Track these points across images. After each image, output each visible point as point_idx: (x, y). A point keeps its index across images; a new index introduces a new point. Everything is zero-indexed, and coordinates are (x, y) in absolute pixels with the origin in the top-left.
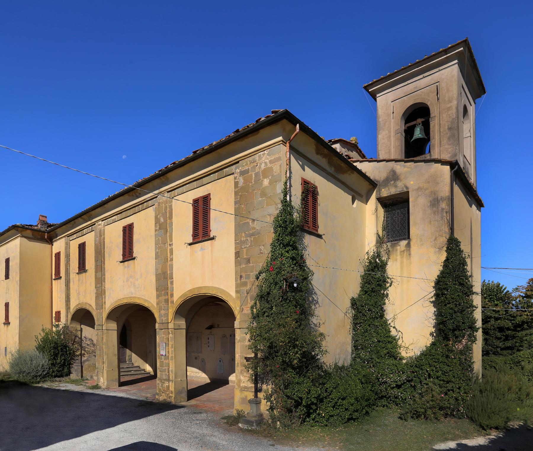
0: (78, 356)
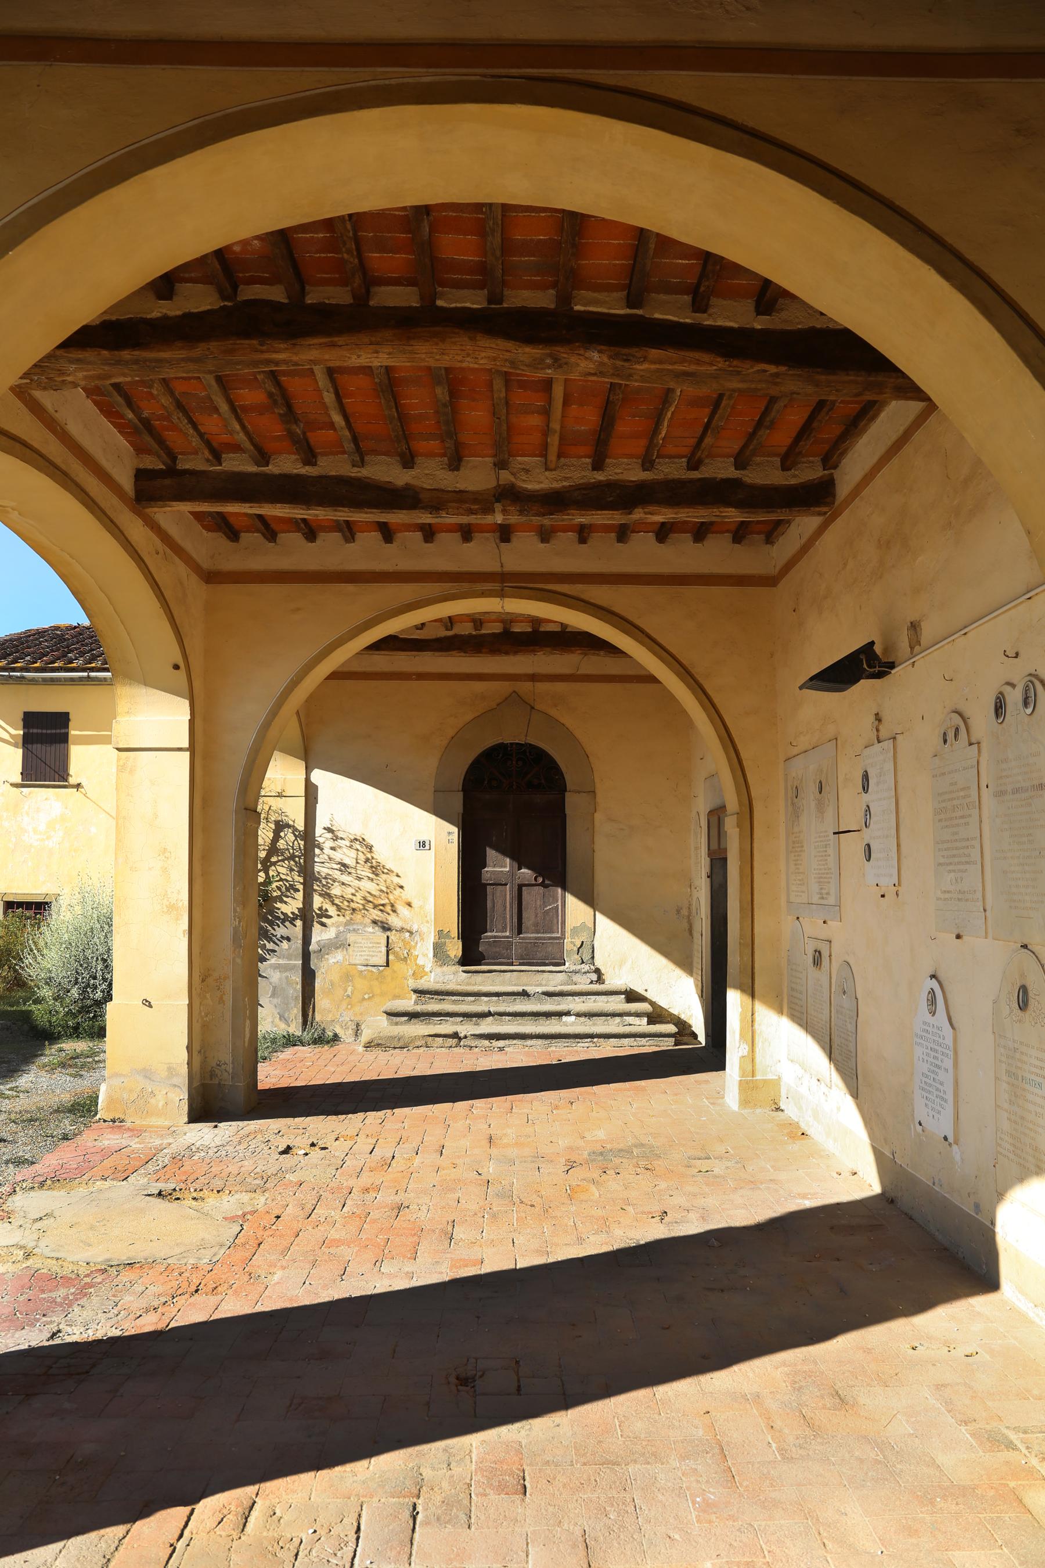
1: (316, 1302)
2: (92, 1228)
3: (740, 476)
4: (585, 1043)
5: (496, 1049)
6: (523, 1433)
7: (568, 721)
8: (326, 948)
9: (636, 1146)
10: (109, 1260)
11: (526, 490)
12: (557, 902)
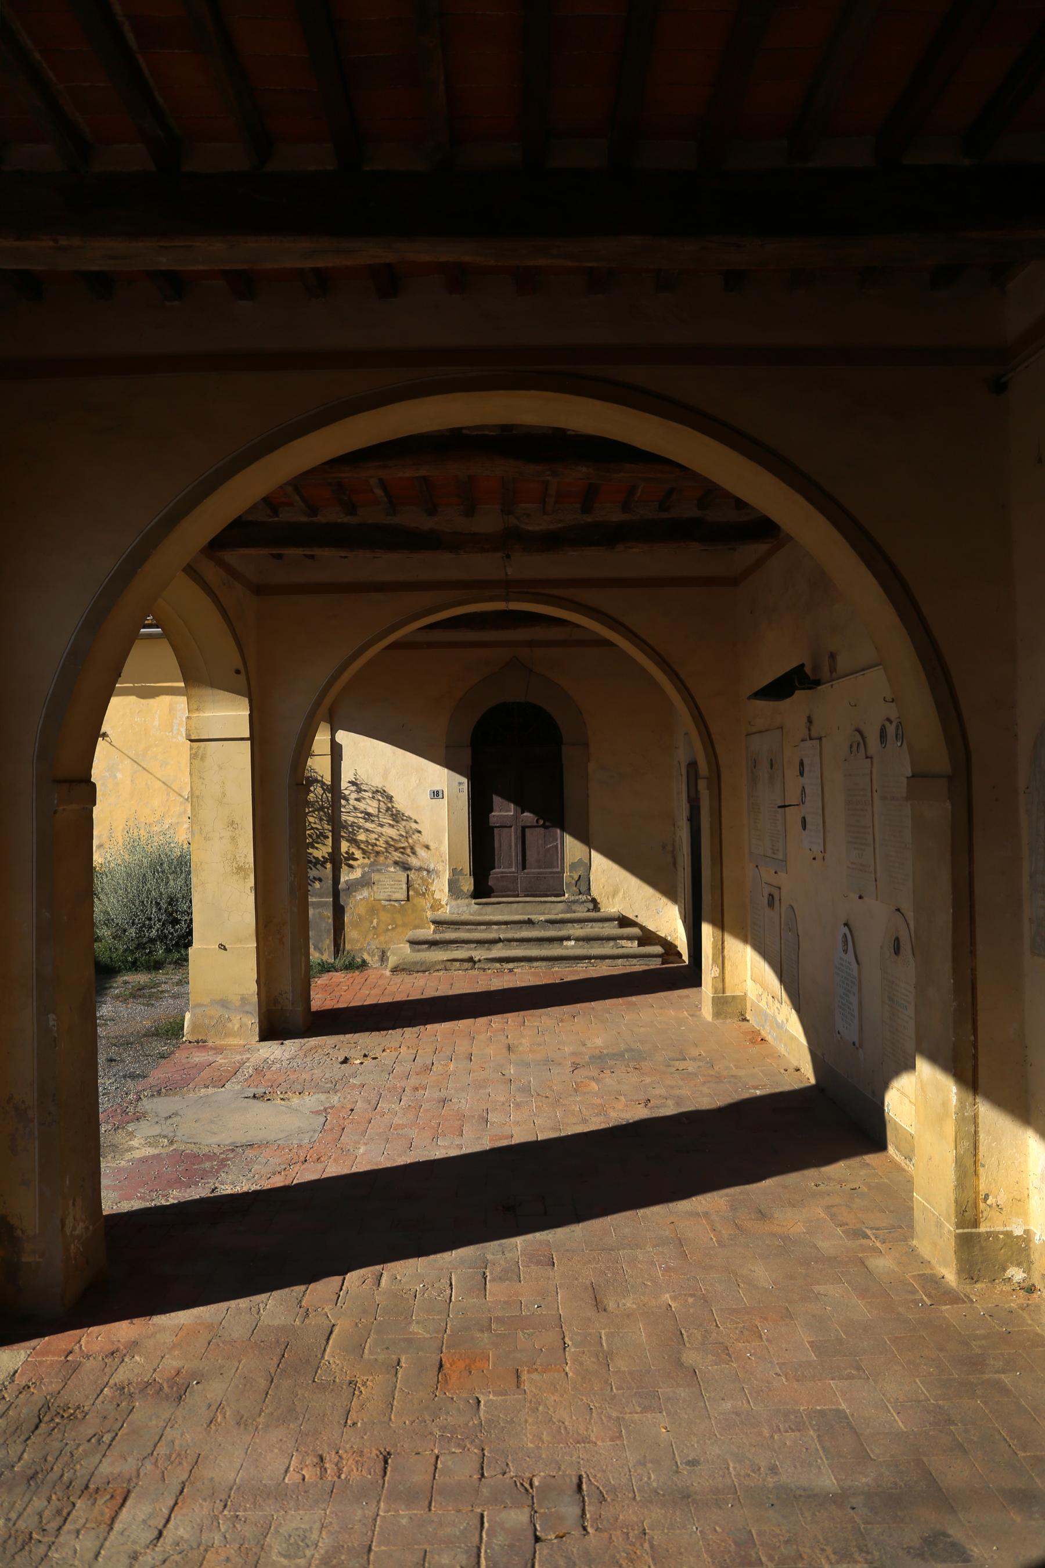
0: (323, 864)
1: (395, 1165)
2: (212, 1122)
6: (550, 1235)
8: (354, 886)
12: (557, 840)
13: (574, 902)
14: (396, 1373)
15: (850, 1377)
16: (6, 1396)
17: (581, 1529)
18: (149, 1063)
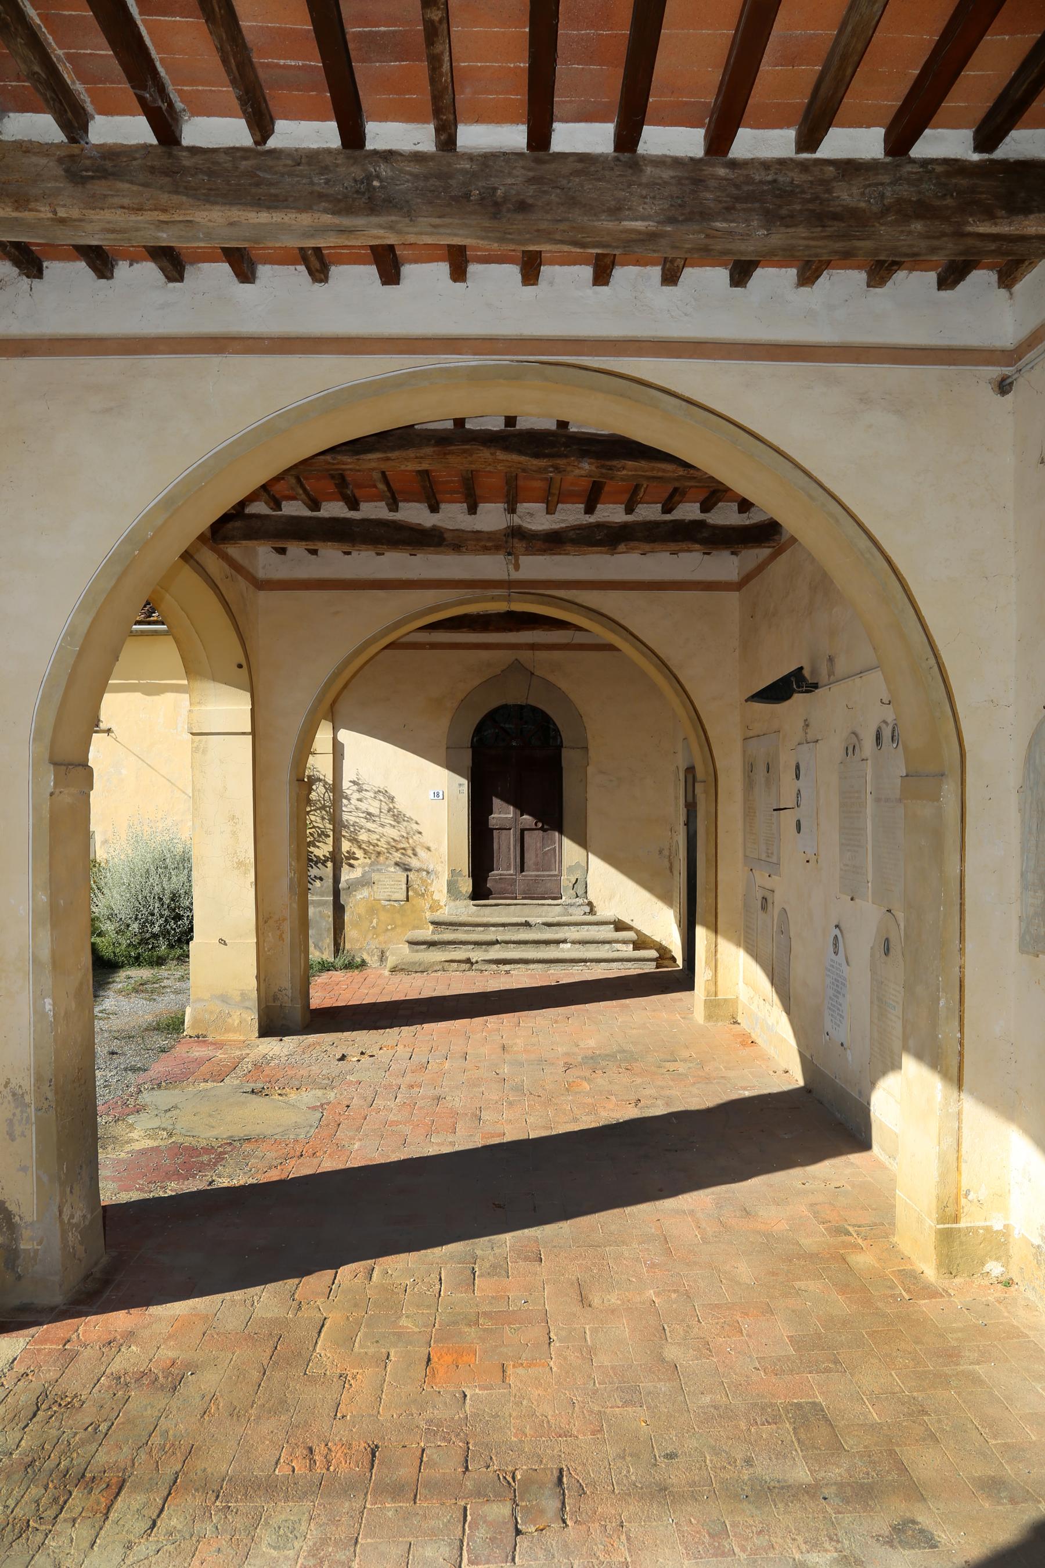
0: (324, 863)
2: (210, 1116)
3: (704, 518)
4: (580, 967)
5: (503, 972)
7: (563, 685)
9: (619, 1052)
10: (232, 1137)
11: (531, 530)
13: (571, 905)
14: (386, 1367)
15: (828, 1370)
16: (5, 1383)
17: (561, 1522)
18: (150, 1056)
